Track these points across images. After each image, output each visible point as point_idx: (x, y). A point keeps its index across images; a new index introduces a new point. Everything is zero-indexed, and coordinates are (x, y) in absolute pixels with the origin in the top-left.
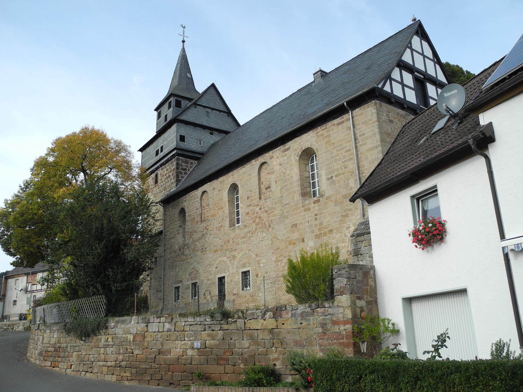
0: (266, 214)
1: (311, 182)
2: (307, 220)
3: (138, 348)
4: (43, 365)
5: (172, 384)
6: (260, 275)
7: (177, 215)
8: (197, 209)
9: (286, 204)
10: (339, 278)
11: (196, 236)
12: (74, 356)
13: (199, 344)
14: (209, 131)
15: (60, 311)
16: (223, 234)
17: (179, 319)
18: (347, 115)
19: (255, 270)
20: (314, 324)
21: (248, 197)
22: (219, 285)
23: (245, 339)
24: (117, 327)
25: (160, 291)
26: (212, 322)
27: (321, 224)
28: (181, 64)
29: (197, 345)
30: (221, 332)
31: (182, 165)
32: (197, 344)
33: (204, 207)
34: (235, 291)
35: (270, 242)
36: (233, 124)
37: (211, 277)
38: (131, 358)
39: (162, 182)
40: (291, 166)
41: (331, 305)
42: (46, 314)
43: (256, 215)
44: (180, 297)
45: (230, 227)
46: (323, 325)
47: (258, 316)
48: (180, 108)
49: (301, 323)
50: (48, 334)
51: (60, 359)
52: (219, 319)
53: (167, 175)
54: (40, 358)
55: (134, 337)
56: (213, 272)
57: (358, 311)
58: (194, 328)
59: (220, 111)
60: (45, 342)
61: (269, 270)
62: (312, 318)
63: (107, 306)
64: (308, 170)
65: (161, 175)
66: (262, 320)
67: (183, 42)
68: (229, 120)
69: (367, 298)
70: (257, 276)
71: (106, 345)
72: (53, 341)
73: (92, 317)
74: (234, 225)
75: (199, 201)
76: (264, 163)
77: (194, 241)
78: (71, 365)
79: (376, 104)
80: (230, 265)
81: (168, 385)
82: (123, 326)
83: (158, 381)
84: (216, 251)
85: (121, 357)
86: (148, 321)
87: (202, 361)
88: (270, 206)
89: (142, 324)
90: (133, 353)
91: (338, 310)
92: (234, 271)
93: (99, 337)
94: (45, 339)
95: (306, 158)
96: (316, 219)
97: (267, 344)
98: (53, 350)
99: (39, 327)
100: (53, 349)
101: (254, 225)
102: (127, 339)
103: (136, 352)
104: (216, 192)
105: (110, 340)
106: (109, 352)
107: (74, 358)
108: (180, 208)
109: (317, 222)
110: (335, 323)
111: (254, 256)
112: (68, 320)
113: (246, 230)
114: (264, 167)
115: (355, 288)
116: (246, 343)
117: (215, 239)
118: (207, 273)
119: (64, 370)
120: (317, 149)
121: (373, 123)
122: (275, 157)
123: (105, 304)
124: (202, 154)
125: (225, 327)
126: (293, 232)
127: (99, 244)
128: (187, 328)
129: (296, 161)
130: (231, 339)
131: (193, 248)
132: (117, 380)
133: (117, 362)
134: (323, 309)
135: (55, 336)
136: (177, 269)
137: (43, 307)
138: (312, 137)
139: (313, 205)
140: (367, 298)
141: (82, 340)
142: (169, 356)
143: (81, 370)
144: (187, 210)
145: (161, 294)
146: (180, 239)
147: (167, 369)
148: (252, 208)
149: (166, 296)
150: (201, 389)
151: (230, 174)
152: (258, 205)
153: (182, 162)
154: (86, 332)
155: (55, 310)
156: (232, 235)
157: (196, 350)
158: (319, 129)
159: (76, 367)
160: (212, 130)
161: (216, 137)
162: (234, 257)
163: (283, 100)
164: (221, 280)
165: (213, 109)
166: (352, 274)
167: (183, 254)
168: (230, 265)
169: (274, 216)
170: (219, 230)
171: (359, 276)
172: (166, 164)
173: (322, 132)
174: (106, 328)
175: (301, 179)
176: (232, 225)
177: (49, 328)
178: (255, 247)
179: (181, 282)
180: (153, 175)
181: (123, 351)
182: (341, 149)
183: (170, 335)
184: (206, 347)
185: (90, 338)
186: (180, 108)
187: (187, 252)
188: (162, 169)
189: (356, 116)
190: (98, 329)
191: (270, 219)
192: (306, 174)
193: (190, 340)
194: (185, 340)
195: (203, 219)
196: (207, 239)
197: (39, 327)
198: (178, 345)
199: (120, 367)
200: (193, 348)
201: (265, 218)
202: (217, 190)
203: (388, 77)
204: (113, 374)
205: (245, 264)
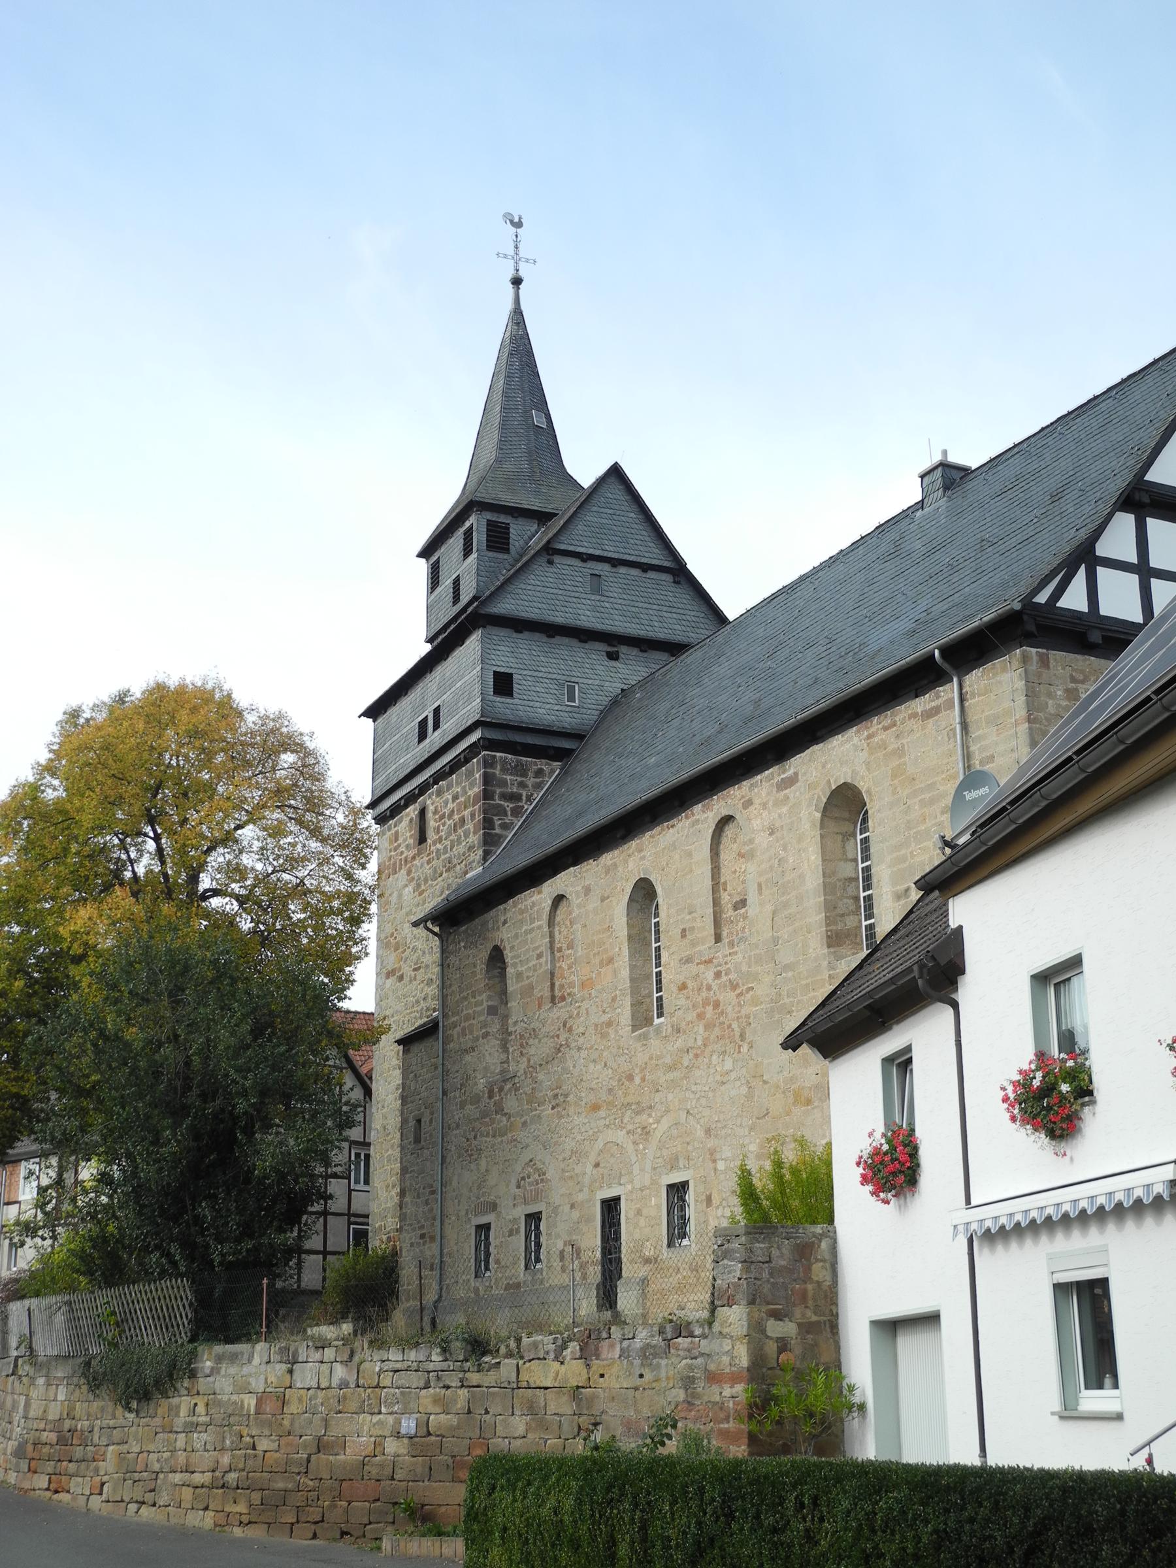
0: (732, 995)
1: (862, 895)
3: (267, 1432)
4: (26, 1485)
5: (347, 1533)
7: (481, 967)
8: (540, 956)
9: (787, 968)
10: (726, 1261)
11: (539, 1050)
12: (109, 1456)
13: (413, 1425)
14: (603, 647)
15: (72, 1321)
16: (614, 1051)
17: (368, 1352)
18: (947, 687)
19: (704, 1180)
20: (668, 1378)
21: (684, 930)
22: (603, 1226)
23: (517, 1412)
24: (218, 1373)
25: (432, 1238)
26: (444, 1365)
28: (509, 376)
29: (409, 1426)
30: (463, 1392)
31: (504, 783)
32: (409, 1425)
33: (560, 950)
34: (649, 1252)
35: (744, 1090)
36: (694, 612)
37: (581, 1197)
38: (250, 1462)
39: (440, 840)
41: (706, 1330)
42: (36, 1326)
43: (704, 994)
44: (492, 1265)
45: (635, 1028)
46: (688, 1382)
47: (548, 1353)
49: (641, 1376)
50: (42, 1389)
51: (72, 1467)
52: (461, 1358)
53: (456, 817)
54: (17, 1464)
55: (259, 1402)
56: (586, 1180)
57: (771, 1348)
58: (402, 1379)
59: (645, 568)
60: (32, 1414)
62: (664, 1362)
63: (196, 1311)
64: (850, 856)
65: (435, 812)
66: (556, 1365)
67: (517, 282)
68: (682, 597)
69: (803, 1315)
70: (709, 1200)
71: (192, 1423)
72: (54, 1413)
73: (153, 1340)
74: (648, 1021)
75: (546, 929)
76: (727, 820)
77: (532, 1068)
78: (103, 1484)
79: (1025, 659)
80: (634, 1159)
81: (338, 1536)
82: (233, 1370)
83: (313, 1527)
84: (596, 1108)
85: (226, 1460)
86: (293, 1357)
87: (419, 1470)
89: (278, 1366)
90: (254, 1448)
91: (721, 1345)
92: (647, 1182)
93: (175, 1401)
94: (34, 1405)
95: (846, 815)
97: (565, 1426)
98: (55, 1441)
99: (16, 1366)
100: (53, 1437)
101: (701, 1029)
102: (242, 1407)
103: (263, 1445)
104: (593, 903)
105: (201, 1409)
106: (198, 1445)
107: (108, 1466)
108: (490, 946)
110: (713, 1378)
111: (700, 1133)
112: (94, 1350)
113: (680, 1043)
114: (729, 831)
115: (766, 1289)
116: (519, 1424)
117: (591, 1066)
118: (571, 1183)
119: (82, 1500)
120: (868, 791)
121: (1016, 724)
123: (191, 1305)
124: (579, 737)
125: (474, 1378)
127: (175, 1126)
128: (386, 1380)
129: (814, 825)
130: (487, 1412)
131: (528, 1090)
132: (216, 1525)
133: (217, 1474)
134: (690, 1339)
135: (61, 1397)
136: (483, 1163)
137: (26, 1302)
138: (856, 747)
140: (803, 1315)
141: (130, 1411)
142: (341, 1457)
143: (127, 1499)
144: (509, 956)
145: (435, 1247)
146: (490, 1056)
147: (336, 1493)
149: (450, 1255)
150: (402, 1544)
151: (634, 844)
153: (503, 770)
154: (139, 1381)
155: (59, 1318)
156: (641, 1058)
157: (406, 1441)
158: (876, 724)
159: (114, 1490)
160: (613, 643)
161: (631, 669)
162: (646, 1132)
163: (833, 560)
164: (611, 1207)
165: (615, 563)
166: (759, 1252)
167: (500, 1110)
168: (634, 1159)
169: (755, 1002)
170: (604, 1036)
171: (782, 1256)
172: (451, 772)
173: (883, 736)
174: (193, 1374)
175: (828, 888)
176: (641, 1020)
177: (44, 1372)
178: (703, 1101)
179: (494, 1207)
180: (412, 811)
181: (232, 1443)
182: (932, 801)
183: (345, 1398)
184: (429, 1434)
185: (152, 1405)
187: (511, 1104)
188: (439, 793)
190: (171, 1376)
192: (847, 870)
193: (391, 1413)
194: (380, 1413)
195: (557, 992)
196: (570, 1064)
197: (16, 1366)
198: (362, 1425)
199: (223, 1487)
200: (398, 1435)
201: (730, 1009)
202: (595, 892)
203: (1085, 557)
204: (206, 1509)
205: (677, 1159)
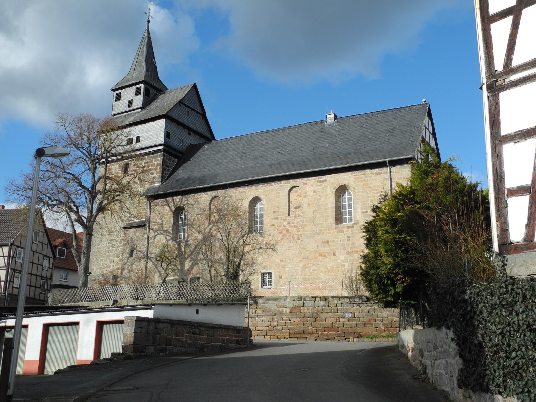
2: (340, 239)
6: (284, 277)
27: (353, 244)
40: (326, 195)
48: (149, 97)
59: (197, 112)
61: (295, 274)
67: (149, 22)
88: (301, 223)
96: (348, 240)
109: (350, 243)
114: (294, 189)
122: (309, 184)
126: (324, 247)
129: (332, 192)
139: (346, 229)
148: (278, 221)
152: (286, 220)
165: (192, 109)
186: (149, 97)
189: (393, 172)
191: (299, 233)
